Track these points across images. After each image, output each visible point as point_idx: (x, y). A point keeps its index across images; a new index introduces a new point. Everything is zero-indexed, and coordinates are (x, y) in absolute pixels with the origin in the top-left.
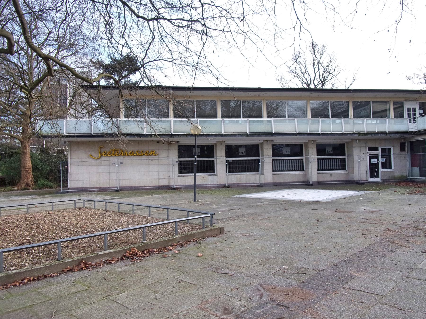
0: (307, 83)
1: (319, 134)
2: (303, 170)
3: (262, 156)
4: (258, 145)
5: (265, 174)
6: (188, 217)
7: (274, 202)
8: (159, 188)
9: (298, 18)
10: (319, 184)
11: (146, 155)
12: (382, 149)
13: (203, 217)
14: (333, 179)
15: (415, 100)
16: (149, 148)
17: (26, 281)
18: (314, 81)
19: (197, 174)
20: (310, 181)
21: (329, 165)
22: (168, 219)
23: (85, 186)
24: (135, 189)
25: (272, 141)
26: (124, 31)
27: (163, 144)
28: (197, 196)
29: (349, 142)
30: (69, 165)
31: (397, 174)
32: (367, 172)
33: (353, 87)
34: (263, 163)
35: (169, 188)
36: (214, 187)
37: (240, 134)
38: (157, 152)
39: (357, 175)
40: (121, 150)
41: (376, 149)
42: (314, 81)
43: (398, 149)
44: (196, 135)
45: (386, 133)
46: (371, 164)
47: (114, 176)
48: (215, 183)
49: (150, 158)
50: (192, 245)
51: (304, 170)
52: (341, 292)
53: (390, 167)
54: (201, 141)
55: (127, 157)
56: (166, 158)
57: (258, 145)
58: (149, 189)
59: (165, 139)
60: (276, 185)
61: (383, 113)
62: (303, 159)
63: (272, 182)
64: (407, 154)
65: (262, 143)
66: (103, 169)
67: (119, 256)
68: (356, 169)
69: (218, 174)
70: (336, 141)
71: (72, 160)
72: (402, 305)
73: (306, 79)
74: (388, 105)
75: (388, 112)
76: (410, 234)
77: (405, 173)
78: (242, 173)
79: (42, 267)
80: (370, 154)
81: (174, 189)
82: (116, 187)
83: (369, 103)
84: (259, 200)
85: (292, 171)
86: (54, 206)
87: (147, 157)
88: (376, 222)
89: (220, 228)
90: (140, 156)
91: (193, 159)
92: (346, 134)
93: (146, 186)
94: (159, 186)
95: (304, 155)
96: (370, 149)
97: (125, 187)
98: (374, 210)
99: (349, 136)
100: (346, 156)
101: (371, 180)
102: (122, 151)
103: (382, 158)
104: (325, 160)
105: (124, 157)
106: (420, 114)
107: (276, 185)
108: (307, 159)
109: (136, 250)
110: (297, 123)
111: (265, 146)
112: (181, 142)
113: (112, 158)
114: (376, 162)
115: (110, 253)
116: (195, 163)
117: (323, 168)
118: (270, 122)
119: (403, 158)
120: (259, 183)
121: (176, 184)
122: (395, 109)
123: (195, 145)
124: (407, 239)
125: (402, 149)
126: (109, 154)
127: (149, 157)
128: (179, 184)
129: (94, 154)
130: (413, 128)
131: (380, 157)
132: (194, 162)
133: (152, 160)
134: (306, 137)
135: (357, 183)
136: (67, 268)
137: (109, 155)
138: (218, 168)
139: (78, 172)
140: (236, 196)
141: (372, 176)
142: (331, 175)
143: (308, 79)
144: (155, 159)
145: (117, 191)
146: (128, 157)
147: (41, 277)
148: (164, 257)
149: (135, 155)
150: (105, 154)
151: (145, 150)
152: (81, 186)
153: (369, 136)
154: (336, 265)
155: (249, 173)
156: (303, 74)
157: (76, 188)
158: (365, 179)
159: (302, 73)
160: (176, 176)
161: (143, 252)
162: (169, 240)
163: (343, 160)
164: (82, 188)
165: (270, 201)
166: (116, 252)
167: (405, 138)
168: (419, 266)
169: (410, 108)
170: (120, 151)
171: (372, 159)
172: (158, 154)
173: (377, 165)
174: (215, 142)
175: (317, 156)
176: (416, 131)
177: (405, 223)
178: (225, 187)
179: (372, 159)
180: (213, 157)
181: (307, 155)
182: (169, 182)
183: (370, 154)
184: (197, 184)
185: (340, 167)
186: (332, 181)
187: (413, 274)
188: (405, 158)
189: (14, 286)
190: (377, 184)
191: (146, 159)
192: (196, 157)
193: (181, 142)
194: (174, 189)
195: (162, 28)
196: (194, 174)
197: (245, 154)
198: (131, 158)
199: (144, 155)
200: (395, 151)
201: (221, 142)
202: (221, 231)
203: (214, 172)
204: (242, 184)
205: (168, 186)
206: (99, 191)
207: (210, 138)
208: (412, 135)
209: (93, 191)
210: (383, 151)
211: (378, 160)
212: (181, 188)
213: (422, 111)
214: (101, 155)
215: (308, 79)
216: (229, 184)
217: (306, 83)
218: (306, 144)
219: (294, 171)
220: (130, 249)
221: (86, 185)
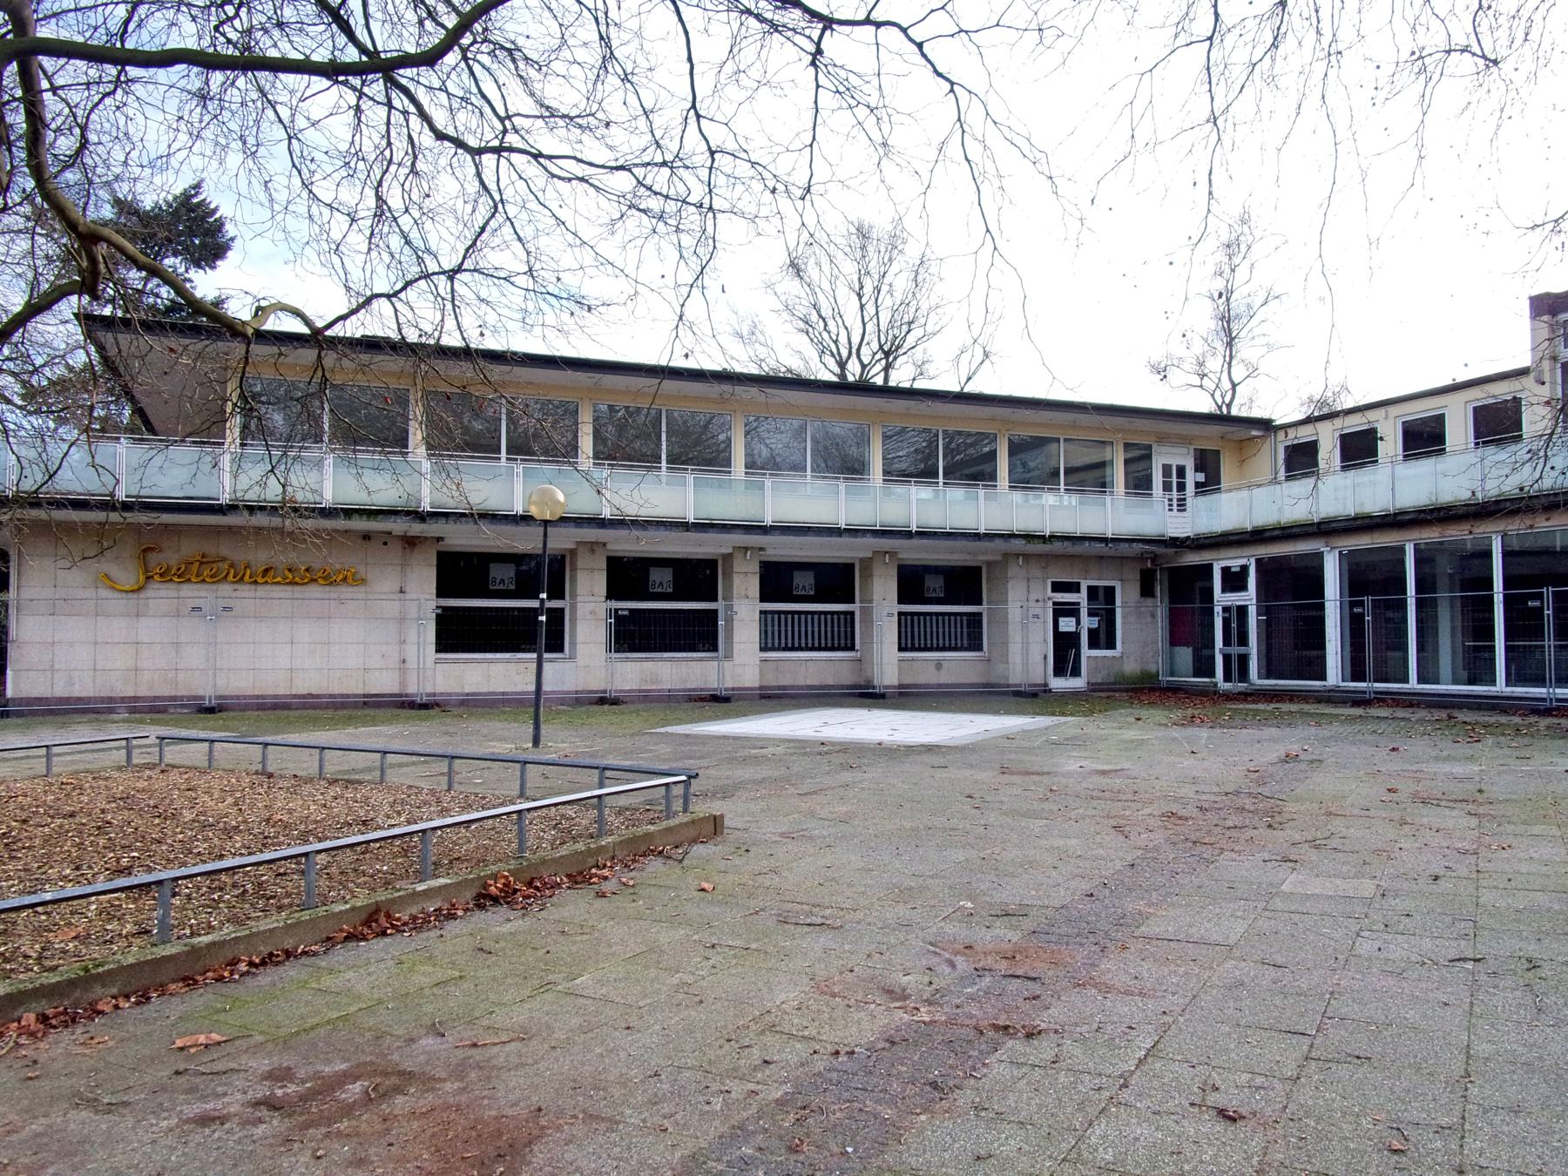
0: (839, 353)
1: (908, 535)
2: (852, 648)
3: (728, 597)
4: (715, 562)
5: (737, 659)
6: (601, 786)
7: (800, 746)
8: (365, 703)
9: (988, 231)
10: (901, 694)
11: (320, 581)
12: (1090, 588)
13: (667, 785)
14: (944, 678)
15: (1184, 440)
16: (318, 559)
17: (243, 967)
18: (858, 350)
19: (546, 655)
20: (875, 683)
21: (786, 631)
22: (522, 795)
23: (77, 691)
24: (275, 707)
25: (761, 549)
26: (384, 173)
27: (385, 544)
28: (544, 729)
29: (995, 562)
30: (12, 611)
31: (1131, 667)
32: (1045, 657)
33: (984, 384)
34: (729, 621)
35: (403, 702)
36: (562, 702)
37: (712, 526)
38: (362, 574)
39: (1019, 668)
40: (224, 559)
41: (1073, 588)
42: (858, 350)
43: (1134, 590)
44: (546, 523)
45: (1105, 540)
47: (194, 657)
48: (565, 689)
49: (333, 595)
50: (654, 865)
51: (857, 647)
52: (1134, 946)
54: (525, 542)
55: (247, 587)
56: (394, 597)
57: (715, 562)
58: (327, 706)
59: (398, 526)
60: (769, 697)
61: (1090, 476)
62: (852, 614)
63: (757, 685)
64: (1159, 607)
65: (731, 555)
67: (469, 894)
68: (1015, 649)
70: (955, 557)
71: (25, 594)
72: (1280, 960)
73: (836, 342)
74: (1108, 449)
75: (1108, 471)
76: (1230, 824)
77: (1156, 665)
78: (658, 655)
79: (275, 925)
80: (1055, 604)
81: (425, 706)
82: (202, 698)
83: (1058, 440)
84: (762, 742)
85: (820, 649)
86: (55, 759)
87: (321, 589)
88: (1130, 796)
89: (715, 817)
90: (296, 584)
91: (534, 604)
92: (989, 536)
93: (318, 696)
94: (365, 696)
95: (857, 598)
96: (1057, 587)
97: (238, 697)
98: (1105, 767)
99: (998, 542)
100: (985, 606)
101: (1058, 684)
102: (232, 566)
103: (1090, 614)
104: (829, 617)
105: (236, 586)
106: (1198, 485)
107: (769, 697)
108: (867, 613)
109: (511, 879)
110: (843, 495)
111: (739, 565)
112: (447, 541)
113: (187, 591)
114: (1073, 629)
115: (446, 886)
116: (540, 618)
117: (913, 644)
118: (762, 487)
119: (1149, 619)
120: (715, 690)
121: (429, 690)
122: (1127, 462)
123: (540, 552)
124: (1228, 833)
125: (1147, 591)
126: (180, 575)
127: (332, 588)
128: (440, 688)
130: (1179, 526)
131: (1084, 612)
132: (535, 612)
133: (341, 601)
134: (870, 541)
135: (1018, 694)
136: (342, 930)
137: (179, 576)
139: (50, 640)
140: (662, 730)
141: (1059, 671)
143: (843, 339)
144: (356, 596)
145: (211, 710)
146: (253, 587)
147: (278, 956)
148: (601, 895)
149: (279, 579)
150: (161, 575)
151: (316, 566)
152: (60, 690)
153: (1057, 546)
154: (1092, 895)
155: (499, 655)
156: (824, 319)
157: (39, 700)
158: (1040, 681)
159: (820, 316)
161: (530, 884)
162: (590, 852)
163: (975, 620)
164: (67, 700)
165: (787, 745)
166: (460, 883)
167: (1156, 556)
168: (1283, 887)
169: (1170, 466)
170: (221, 564)
171: (1061, 619)
172: (363, 581)
174: (572, 546)
175: (900, 602)
176: (1188, 538)
177: (1204, 797)
178: (602, 701)
179: (1061, 619)
182: (403, 683)
183: (1055, 604)
184: (546, 688)
185: (965, 642)
186: (940, 686)
187: (1278, 904)
188: (1153, 616)
189: (217, 980)
190: (1074, 695)
191: (318, 595)
192: (544, 596)
193: (447, 541)
194: (425, 706)
195: (521, 185)
196: (534, 655)
197: (513, 587)
198: (262, 591)
199: (313, 580)
200: (1126, 596)
201: (593, 546)
202: (715, 825)
204: (659, 691)
205: (400, 695)
206: (133, 710)
208: (1177, 547)
209: (111, 711)
210: (1093, 592)
211: (1078, 623)
212: (447, 702)
213: (1201, 477)
215: (843, 339)
216: (616, 691)
217: (833, 355)
218: (867, 564)
219: (826, 649)
220: (495, 877)
221: (83, 687)
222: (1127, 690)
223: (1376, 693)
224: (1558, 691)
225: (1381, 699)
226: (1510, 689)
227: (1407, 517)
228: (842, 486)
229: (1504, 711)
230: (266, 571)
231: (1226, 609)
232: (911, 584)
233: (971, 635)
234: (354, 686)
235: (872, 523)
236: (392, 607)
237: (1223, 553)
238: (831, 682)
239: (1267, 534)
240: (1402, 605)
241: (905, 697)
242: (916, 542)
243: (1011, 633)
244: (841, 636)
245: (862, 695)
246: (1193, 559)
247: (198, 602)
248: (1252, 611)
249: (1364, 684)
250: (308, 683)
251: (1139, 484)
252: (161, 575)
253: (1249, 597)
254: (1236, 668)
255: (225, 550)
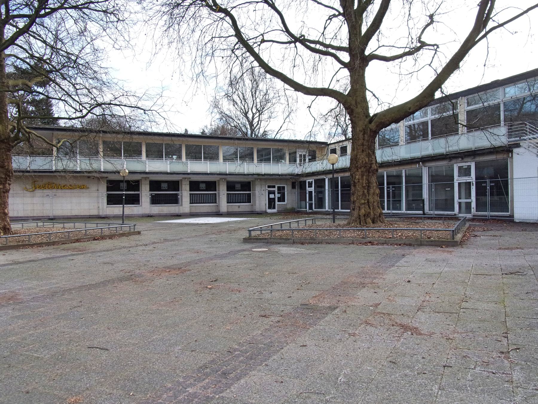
2: (216, 203)
14: (240, 210)
15: (304, 148)
16: (80, 183)
19: (125, 205)
23: (20, 215)
31: (289, 206)
34: (182, 196)
38: (88, 186)
40: (54, 183)
41: (274, 187)
43: (290, 187)
46: (269, 199)
48: (139, 213)
53: (284, 201)
62: (216, 194)
66: (36, 200)
69: (143, 206)
73: (244, 107)
77: (295, 206)
82: (50, 216)
93: (78, 216)
96: (269, 187)
101: (269, 211)
103: (278, 193)
106: (309, 159)
108: (219, 193)
111: (184, 183)
113: (45, 191)
125: (293, 187)
126: (44, 187)
128: (108, 213)
129: (28, 187)
131: (276, 193)
134: (216, 176)
135: (258, 213)
138: (143, 200)
142: (239, 207)
145: (52, 219)
153: (266, 177)
155: (116, 206)
158: (264, 210)
160: (105, 207)
163: (249, 195)
172: (88, 188)
173: (274, 199)
178: (148, 216)
180: (139, 191)
181: (219, 191)
182: (99, 212)
184: (125, 213)
190: (272, 214)
194: (104, 218)
196: (122, 206)
198: (64, 191)
201: (146, 178)
203: (139, 204)
207: (136, 175)
209: (28, 220)
211: (275, 195)
213: (310, 157)
214: (36, 188)
221: (21, 214)
222: (284, 212)
223: (491, 216)
224: (491, 213)
225: (394, 215)
226: (477, 213)
227: (415, 160)
228: (208, 162)
229: (327, 214)
230: (64, 186)
231: (459, 184)
232: (231, 187)
233: (248, 199)
234: (87, 213)
235: (216, 171)
236: (96, 194)
237: (308, 178)
238: (210, 211)
239: (479, 152)
240: (338, 191)
241: (229, 214)
242: (228, 176)
243: (256, 199)
244: (214, 199)
245: (217, 214)
246: (302, 179)
247: (48, 194)
248: (313, 192)
249: (487, 213)
250: (75, 213)
251: (293, 160)
252: (39, 187)
253: (312, 189)
254: (311, 208)
255: (54, 181)
